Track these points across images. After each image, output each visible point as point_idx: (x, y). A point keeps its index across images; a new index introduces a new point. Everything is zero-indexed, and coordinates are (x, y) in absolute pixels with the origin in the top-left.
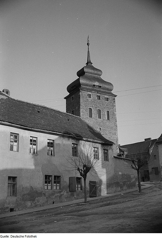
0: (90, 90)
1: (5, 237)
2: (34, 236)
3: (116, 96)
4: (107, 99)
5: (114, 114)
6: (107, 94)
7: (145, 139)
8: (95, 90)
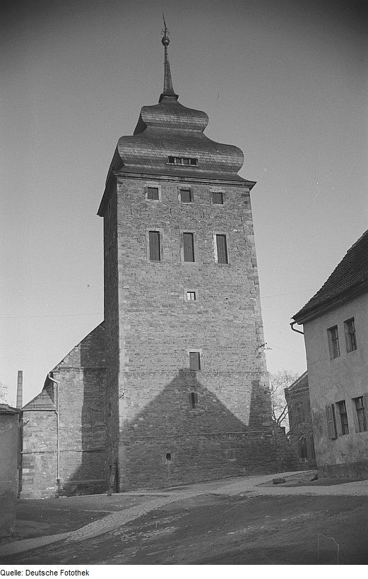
0: (154, 175)
1: (12, 573)
2: (83, 572)
3: (251, 185)
4: (220, 198)
5: (246, 244)
6: (217, 181)
7: (100, 213)
8: (173, 174)
